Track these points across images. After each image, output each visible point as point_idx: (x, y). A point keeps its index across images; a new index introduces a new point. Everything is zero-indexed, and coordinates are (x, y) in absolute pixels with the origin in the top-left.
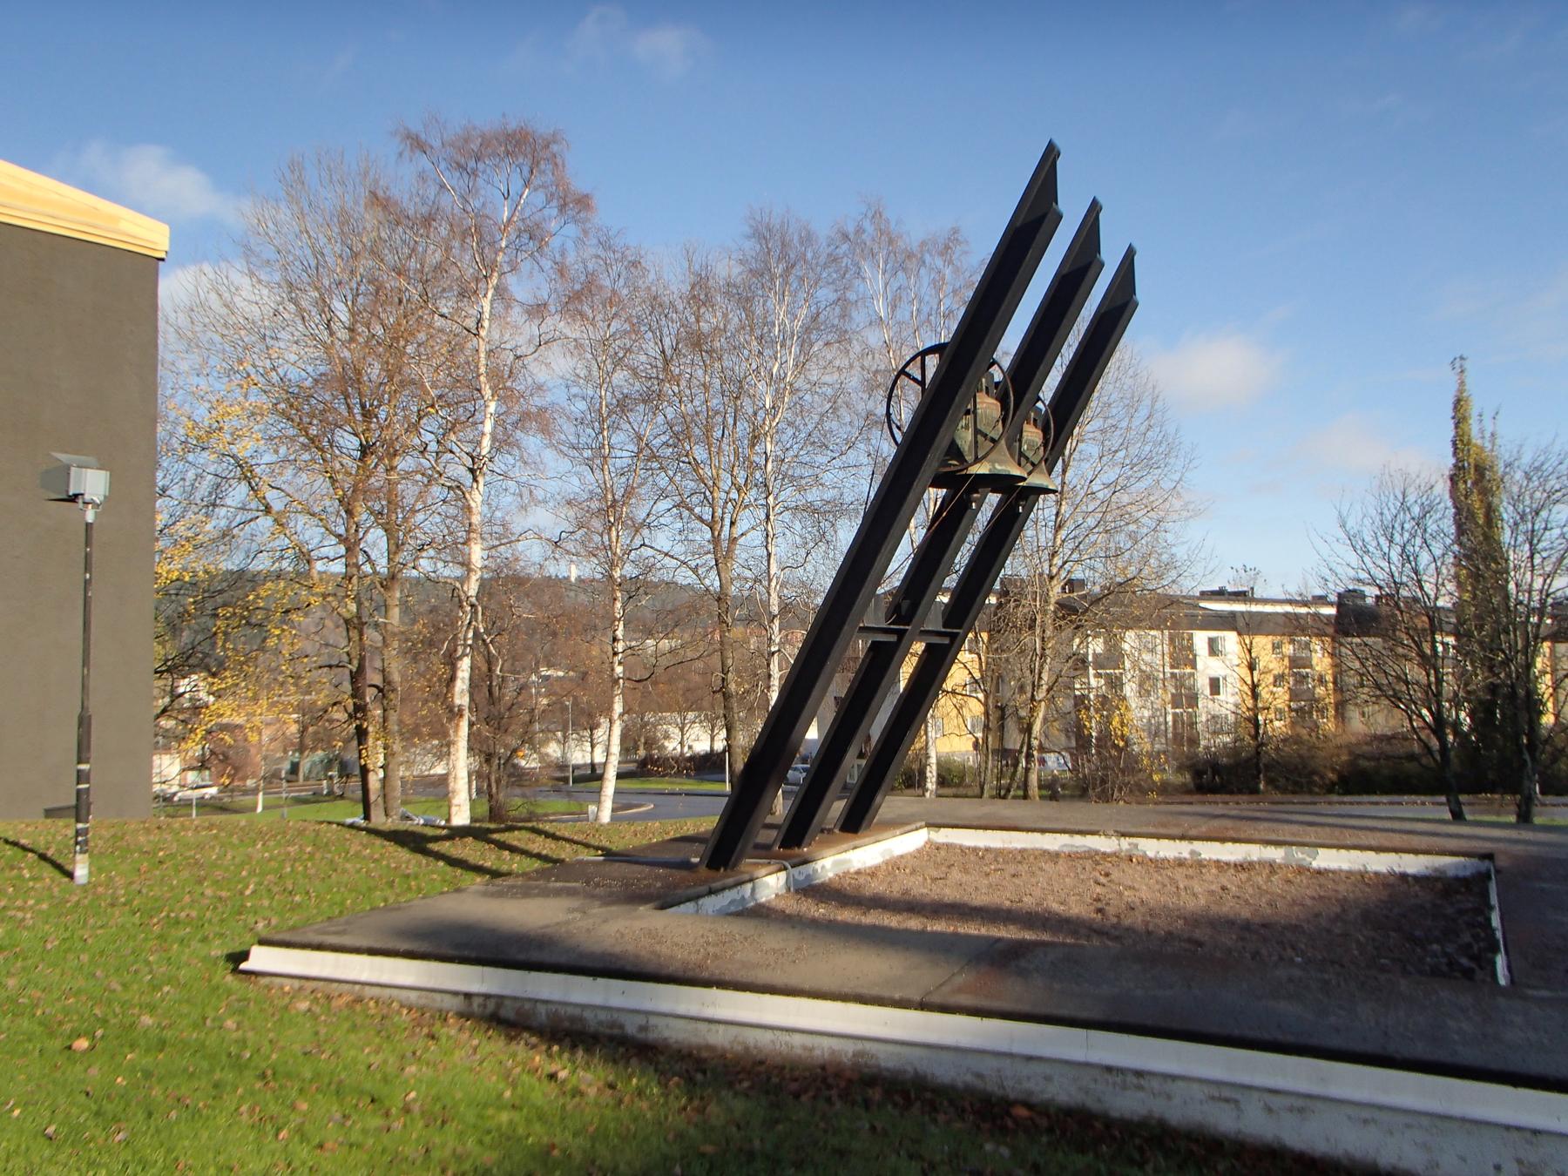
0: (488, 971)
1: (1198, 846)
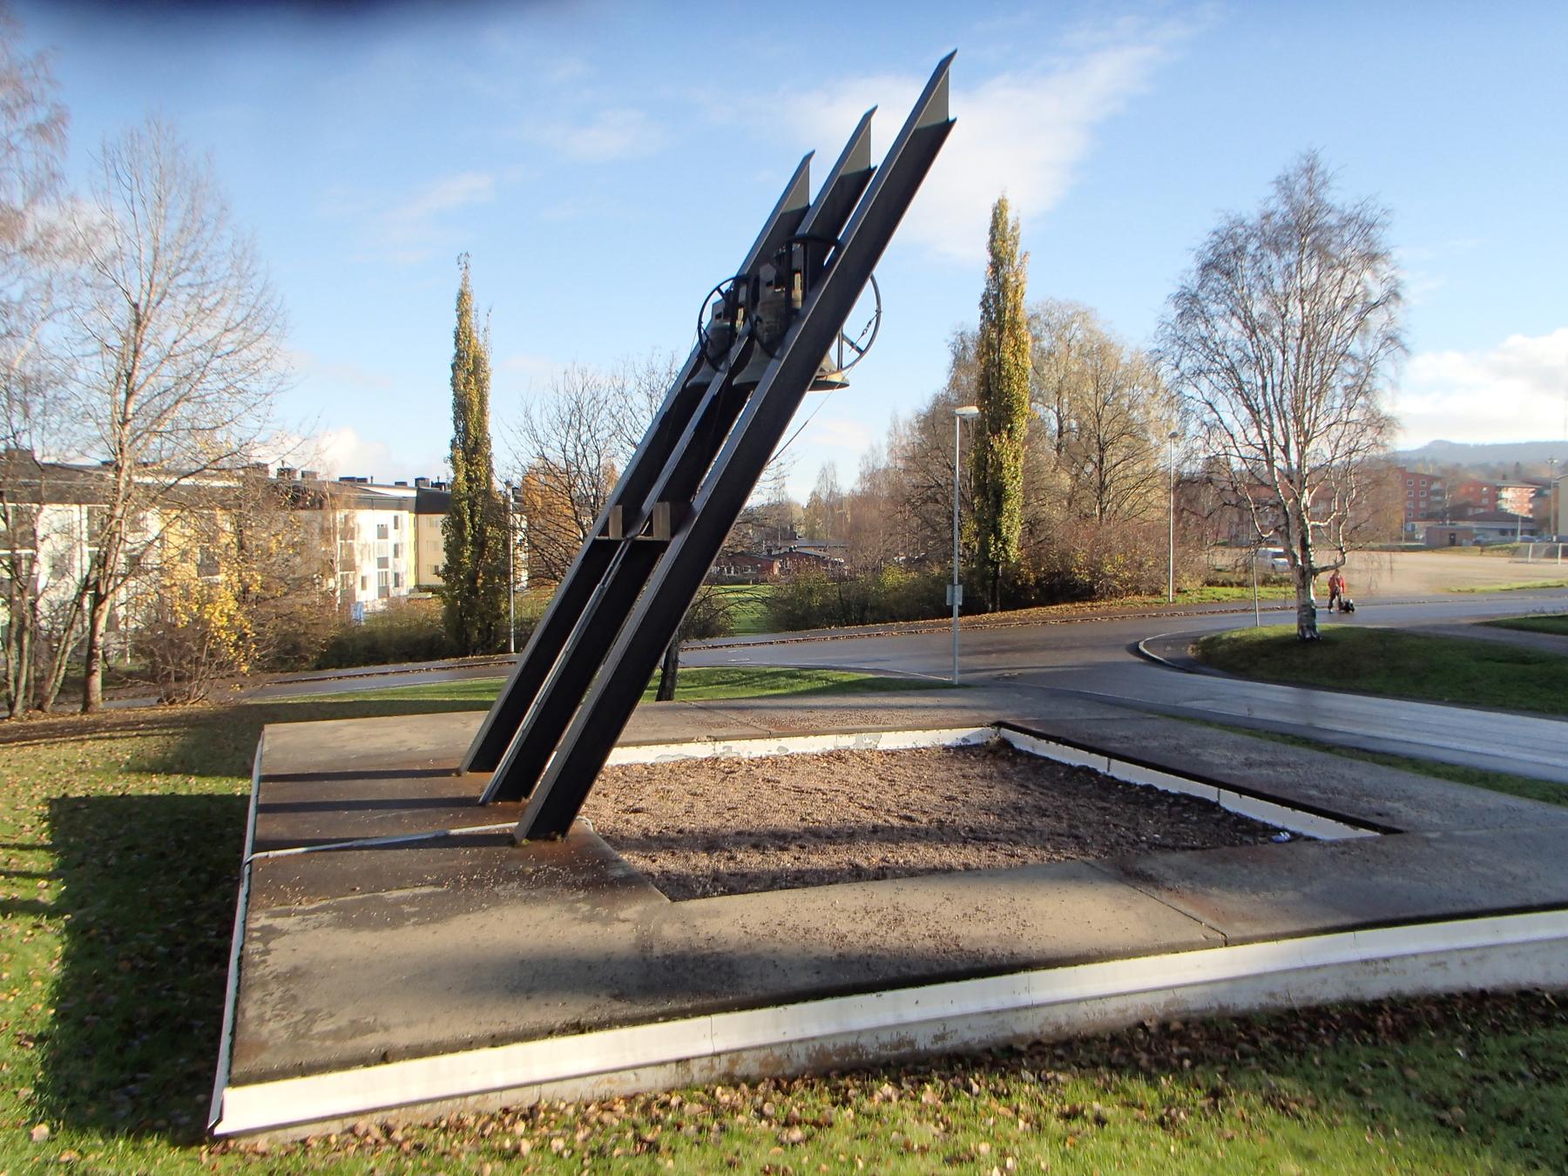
0: (719, 1019)
1: (785, 742)
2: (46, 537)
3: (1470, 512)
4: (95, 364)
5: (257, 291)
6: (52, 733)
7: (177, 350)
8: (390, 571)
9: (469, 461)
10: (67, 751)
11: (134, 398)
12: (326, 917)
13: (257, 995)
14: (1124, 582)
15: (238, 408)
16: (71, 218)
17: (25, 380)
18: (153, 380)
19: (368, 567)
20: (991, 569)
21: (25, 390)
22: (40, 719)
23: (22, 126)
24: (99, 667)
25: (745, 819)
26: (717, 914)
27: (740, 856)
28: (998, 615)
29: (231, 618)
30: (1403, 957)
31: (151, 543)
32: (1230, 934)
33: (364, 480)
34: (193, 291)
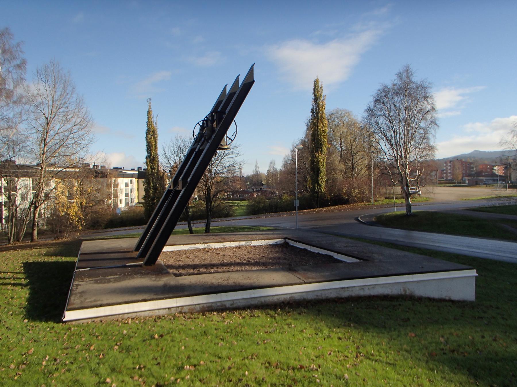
1: (225, 243)
2: (20, 189)
3: (483, 174)
4: (35, 136)
5: (84, 113)
6: (22, 248)
7: (59, 131)
8: (129, 197)
9: (151, 162)
10: (28, 251)
11: (47, 146)
12: (92, 282)
13: (74, 296)
14: (358, 198)
15: (78, 149)
16: (27, 92)
17: (13, 141)
18: (52, 140)
19: (122, 197)
20: (316, 195)
21: (12, 144)
22: (18, 244)
23: (12, 65)
24: (36, 229)
25: (207, 262)
26: (185, 279)
27: (200, 270)
28: (319, 209)
29: (76, 213)
30: (352, 287)
31: (52, 190)
32: (306, 281)
33: (121, 168)
34: (64, 114)
